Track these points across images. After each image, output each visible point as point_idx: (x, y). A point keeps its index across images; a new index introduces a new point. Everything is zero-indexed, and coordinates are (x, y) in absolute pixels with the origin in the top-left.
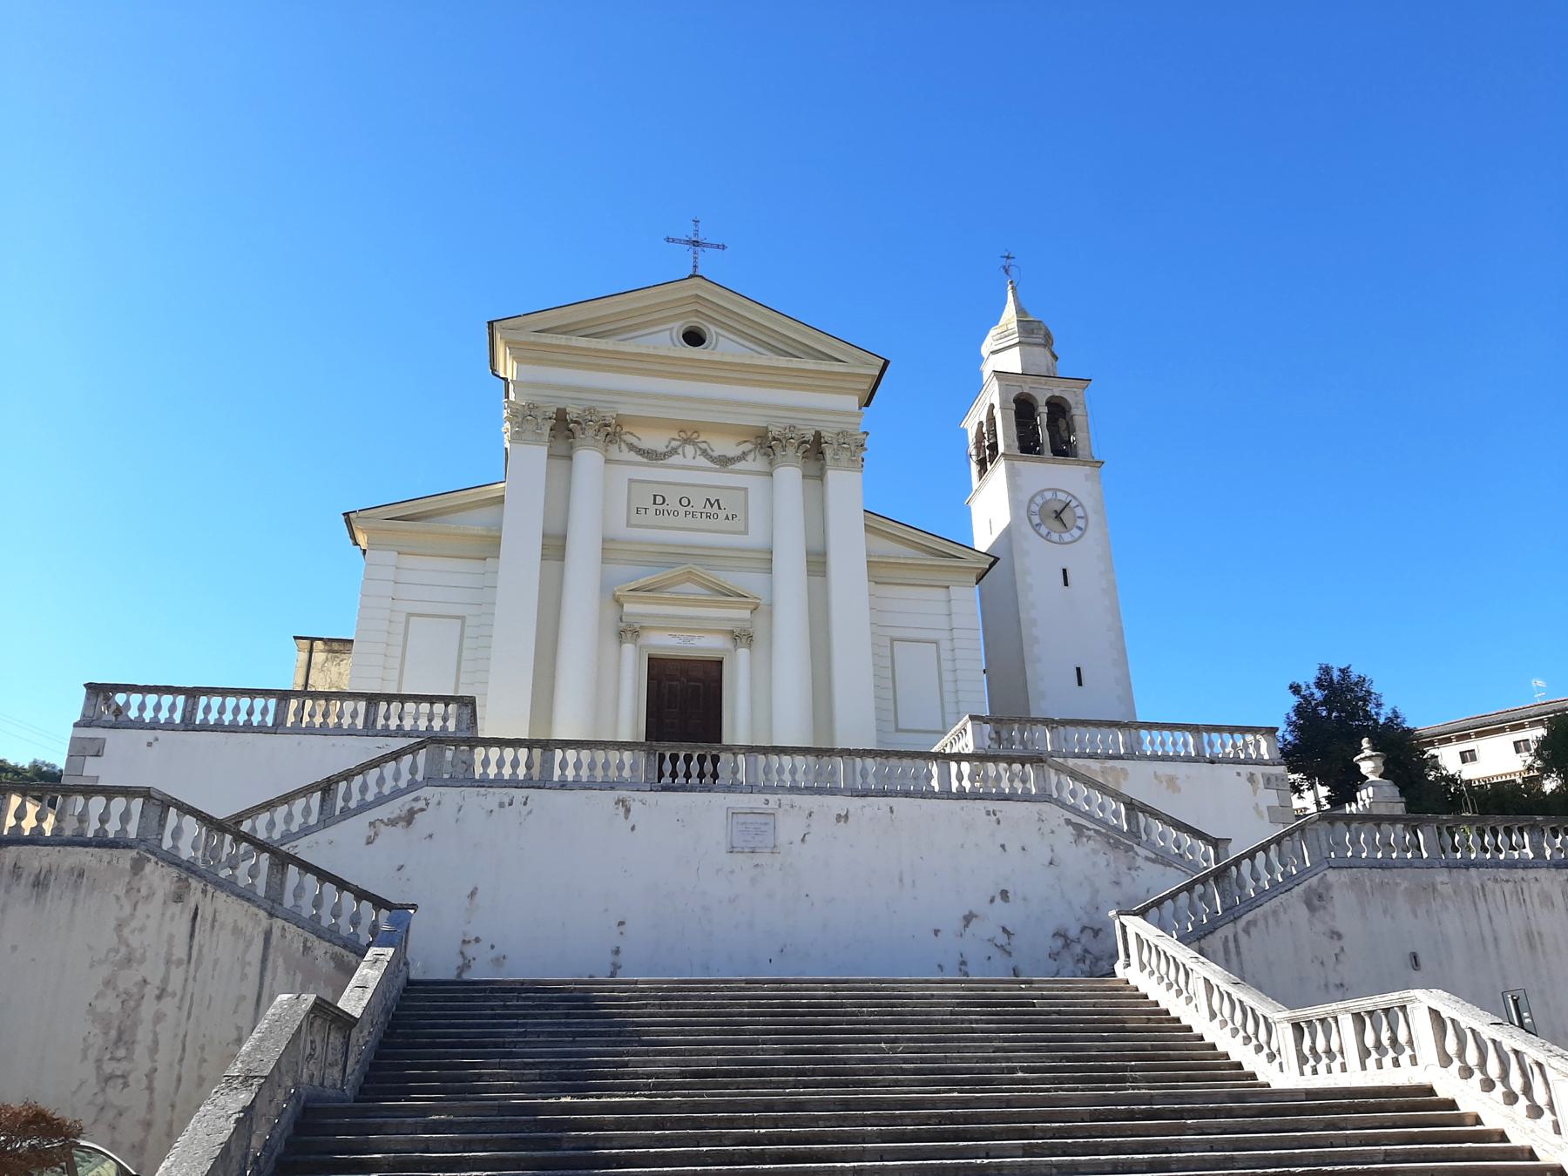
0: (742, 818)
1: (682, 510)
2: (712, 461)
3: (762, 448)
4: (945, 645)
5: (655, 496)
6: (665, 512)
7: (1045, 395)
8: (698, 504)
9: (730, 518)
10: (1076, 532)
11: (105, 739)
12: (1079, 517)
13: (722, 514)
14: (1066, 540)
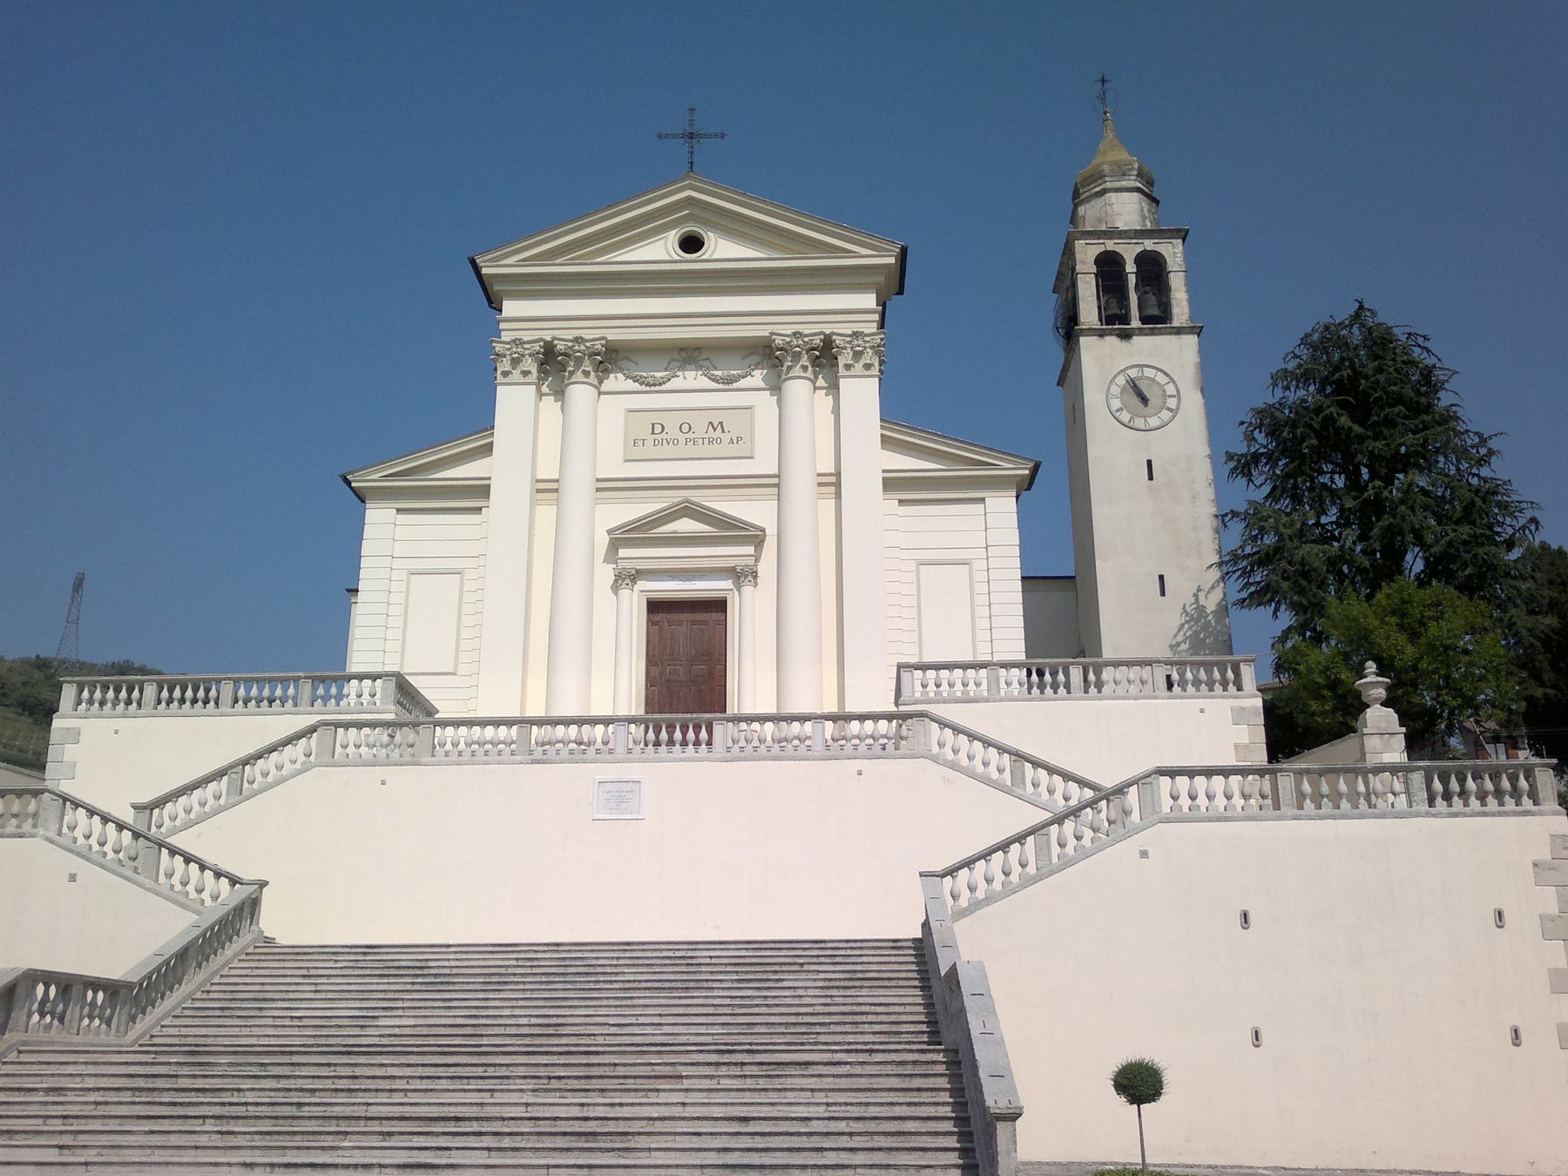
0: (610, 787)
1: (682, 438)
2: (717, 381)
3: (770, 359)
4: (980, 565)
5: (653, 425)
6: (664, 441)
7: (1135, 251)
8: (700, 430)
9: (735, 442)
10: (1165, 415)
11: (80, 728)
12: (1170, 396)
13: (726, 438)
14: (1136, 426)
